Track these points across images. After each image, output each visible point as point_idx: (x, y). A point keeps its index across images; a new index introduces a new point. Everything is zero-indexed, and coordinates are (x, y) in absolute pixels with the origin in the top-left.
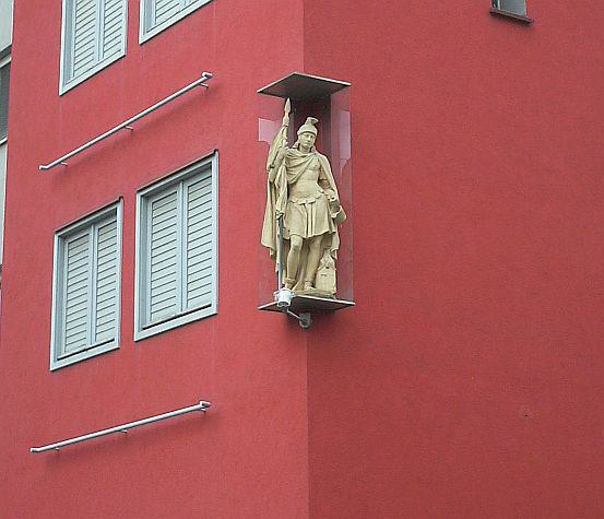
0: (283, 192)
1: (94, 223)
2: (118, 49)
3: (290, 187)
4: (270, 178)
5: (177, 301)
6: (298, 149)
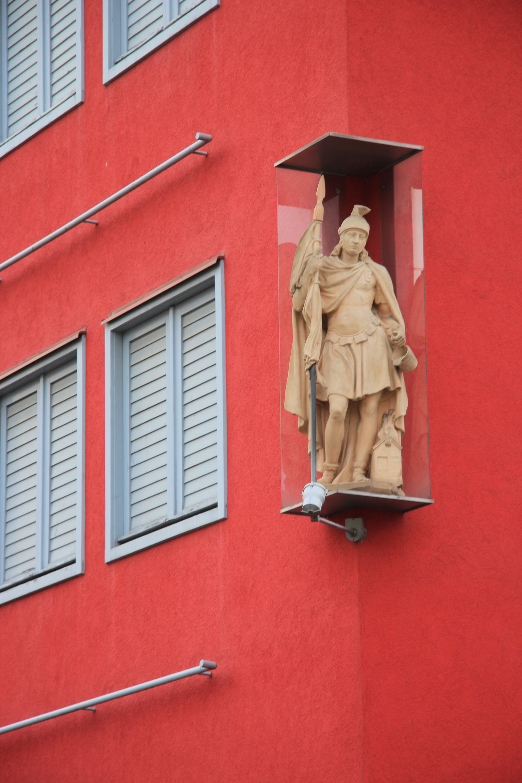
0: (315, 325)
1: (175, 304)
2: (71, 92)
3: (326, 318)
4: (295, 306)
5: (168, 498)
6: (340, 256)
